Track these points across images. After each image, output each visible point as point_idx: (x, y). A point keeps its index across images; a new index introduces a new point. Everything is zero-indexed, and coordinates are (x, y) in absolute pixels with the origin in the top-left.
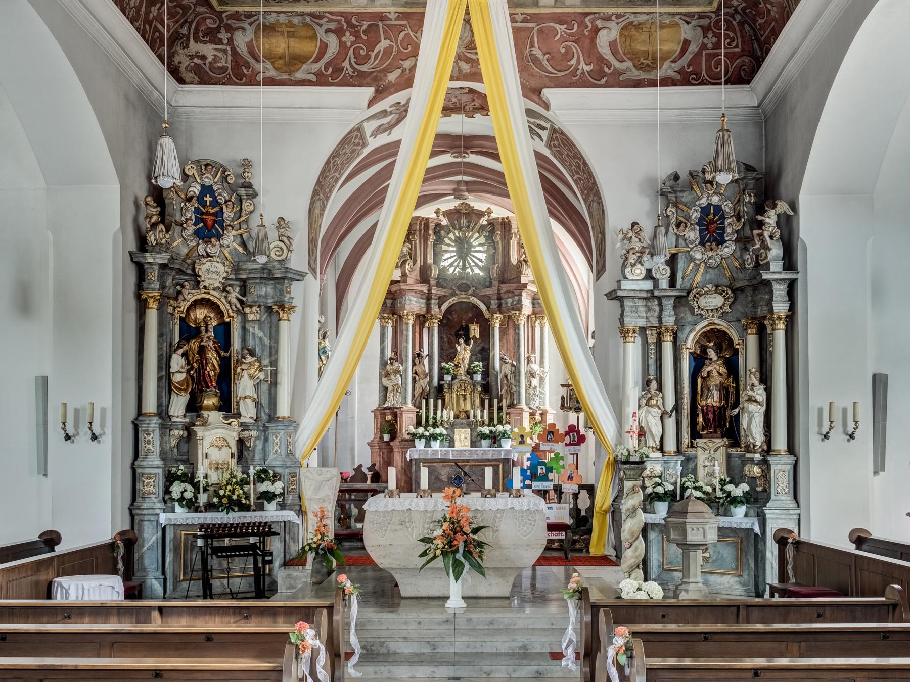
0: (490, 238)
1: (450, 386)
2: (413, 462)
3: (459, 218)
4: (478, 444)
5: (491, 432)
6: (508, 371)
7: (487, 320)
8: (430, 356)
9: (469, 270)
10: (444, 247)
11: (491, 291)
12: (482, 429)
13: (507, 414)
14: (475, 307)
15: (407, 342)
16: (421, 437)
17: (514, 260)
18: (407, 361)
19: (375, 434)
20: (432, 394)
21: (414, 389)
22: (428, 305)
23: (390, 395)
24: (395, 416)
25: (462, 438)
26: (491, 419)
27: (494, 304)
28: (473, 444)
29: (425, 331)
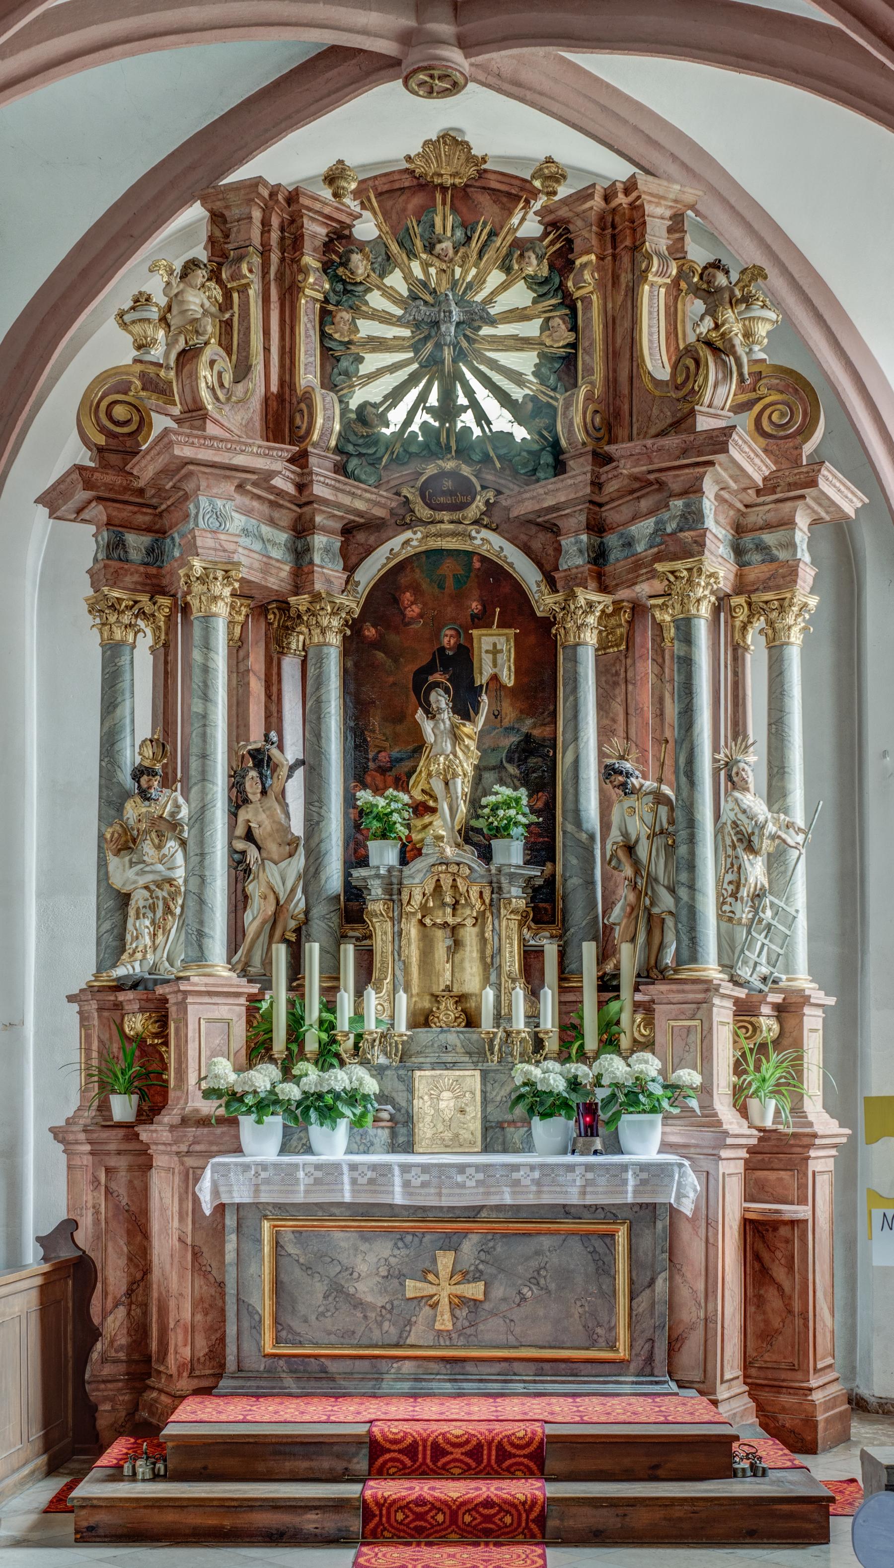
0: (556, 287)
1: (394, 890)
2: (230, 1221)
3: (430, 208)
4: (516, 1135)
5: (574, 1084)
6: (638, 828)
7: (546, 624)
8: (312, 765)
9: (467, 419)
10: (367, 328)
11: (565, 491)
12: (536, 1073)
13: (637, 1006)
14: (494, 574)
15: (206, 697)
16: (265, 1105)
17: (657, 362)
18: (205, 777)
19: (84, 1091)
20: (318, 926)
21: (239, 901)
22: (300, 554)
23: (140, 928)
24: (161, 1014)
25: (448, 1098)
26: (570, 1031)
27: (574, 552)
28: (494, 1136)
29: (290, 667)
